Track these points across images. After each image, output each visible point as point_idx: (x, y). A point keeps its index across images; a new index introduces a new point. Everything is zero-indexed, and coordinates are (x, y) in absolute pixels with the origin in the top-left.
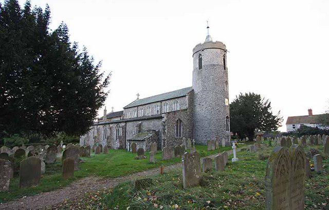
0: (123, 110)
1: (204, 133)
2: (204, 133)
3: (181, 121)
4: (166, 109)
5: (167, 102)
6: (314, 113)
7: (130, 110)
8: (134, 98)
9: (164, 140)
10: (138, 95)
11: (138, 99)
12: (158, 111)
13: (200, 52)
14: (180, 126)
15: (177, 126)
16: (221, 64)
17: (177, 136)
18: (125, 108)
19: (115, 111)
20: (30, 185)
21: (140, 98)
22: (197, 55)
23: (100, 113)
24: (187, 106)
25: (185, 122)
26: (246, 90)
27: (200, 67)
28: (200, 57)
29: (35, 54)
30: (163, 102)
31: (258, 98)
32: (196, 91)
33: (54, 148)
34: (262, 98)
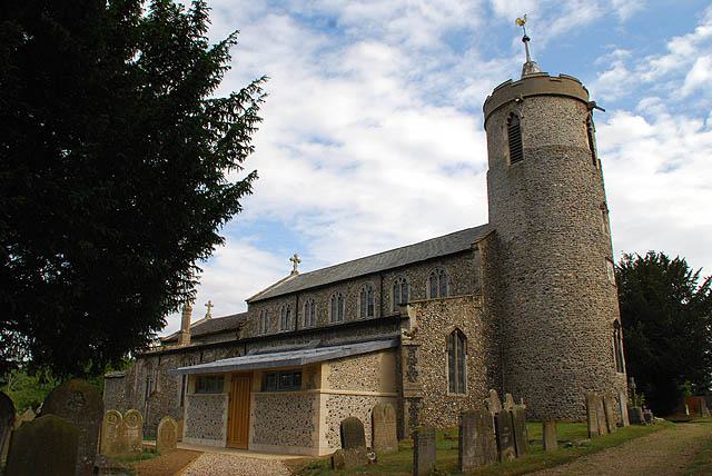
1: (545, 379)
2: (545, 379)
3: (462, 336)
4: (277, 447)
5: (403, 275)
7: (270, 308)
10: (296, 260)
12: (371, 307)
17: (453, 389)
18: (252, 303)
19: (217, 314)
22: (504, 117)
23: (173, 322)
25: (475, 341)
26: (640, 250)
27: (516, 153)
28: (514, 123)
29: (173, 271)
30: (390, 278)
31: (679, 267)
32: (507, 235)
34: (692, 267)
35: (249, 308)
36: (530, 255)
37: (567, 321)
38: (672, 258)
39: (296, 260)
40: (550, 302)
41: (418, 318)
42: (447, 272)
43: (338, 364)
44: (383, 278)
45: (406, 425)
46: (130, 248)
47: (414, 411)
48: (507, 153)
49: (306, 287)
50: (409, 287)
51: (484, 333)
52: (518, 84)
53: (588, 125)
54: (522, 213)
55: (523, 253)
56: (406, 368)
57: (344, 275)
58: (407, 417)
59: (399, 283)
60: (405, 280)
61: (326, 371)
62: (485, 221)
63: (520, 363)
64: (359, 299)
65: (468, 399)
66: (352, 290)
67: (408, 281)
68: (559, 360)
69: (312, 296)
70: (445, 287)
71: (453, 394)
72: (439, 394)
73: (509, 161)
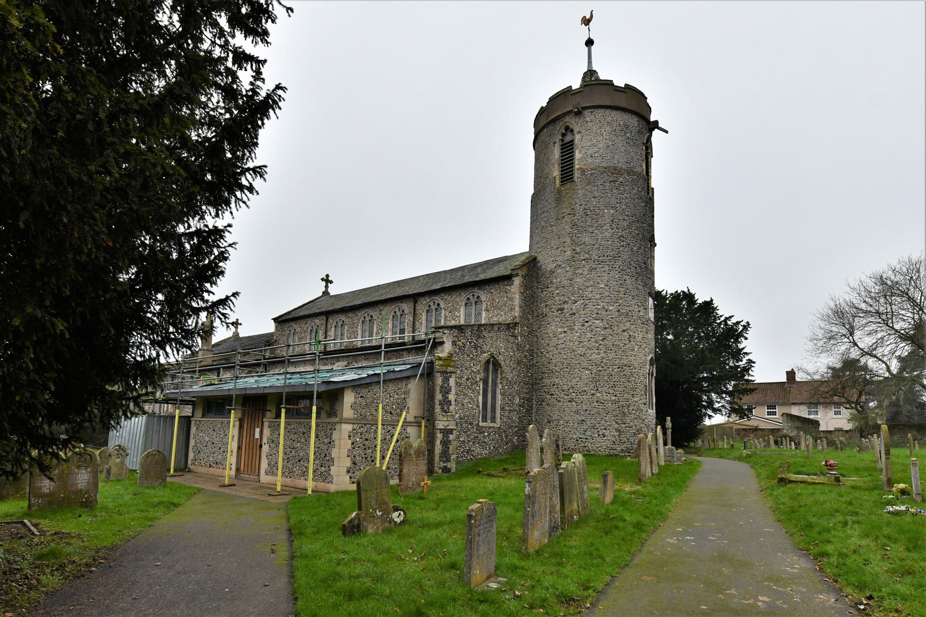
0: (270, 328)
1: (577, 412)
3: (497, 365)
5: (437, 299)
6: (799, 377)
7: (296, 326)
8: (316, 291)
9: (447, 432)
10: (327, 280)
11: (326, 293)
13: (572, 121)
14: (495, 384)
15: (485, 382)
16: (638, 169)
17: (485, 419)
18: (280, 321)
20: (491, 289)
21: (334, 290)
24: (517, 312)
25: (509, 370)
27: (567, 175)
28: (568, 138)
33: (355, 604)
35: (276, 327)
36: (571, 285)
37: (604, 355)
38: (700, 298)
39: (327, 280)
40: (589, 335)
41: (454, 343)
42: (483, 298)
43: (364, 391)
44: (415, 302)
45: (437, 459)
46: (662, 323)
47: (446, 443)
48: (556, 173)
49: (426, 290)
50: (443, 311)
51: (519, 363)
52: (578, 92)
53: (647, 148)
54: (568, 240)
55: (566, 283)
56: (439, 397)
57: (399, 292)
58: (438, 448)
59: (433, 307)
60: (438, 305)
61: (349, 398)
62: (527, 250)
63: (552, 395)
64: (390, 323)
65: (499, 428)
66: (383, 313)
67: (442, 306)
68: (593, 394)
69: (343, 317)
70: (480, 314)
71: (484, 424)
72: (471, 424)
73: (558, 182)
